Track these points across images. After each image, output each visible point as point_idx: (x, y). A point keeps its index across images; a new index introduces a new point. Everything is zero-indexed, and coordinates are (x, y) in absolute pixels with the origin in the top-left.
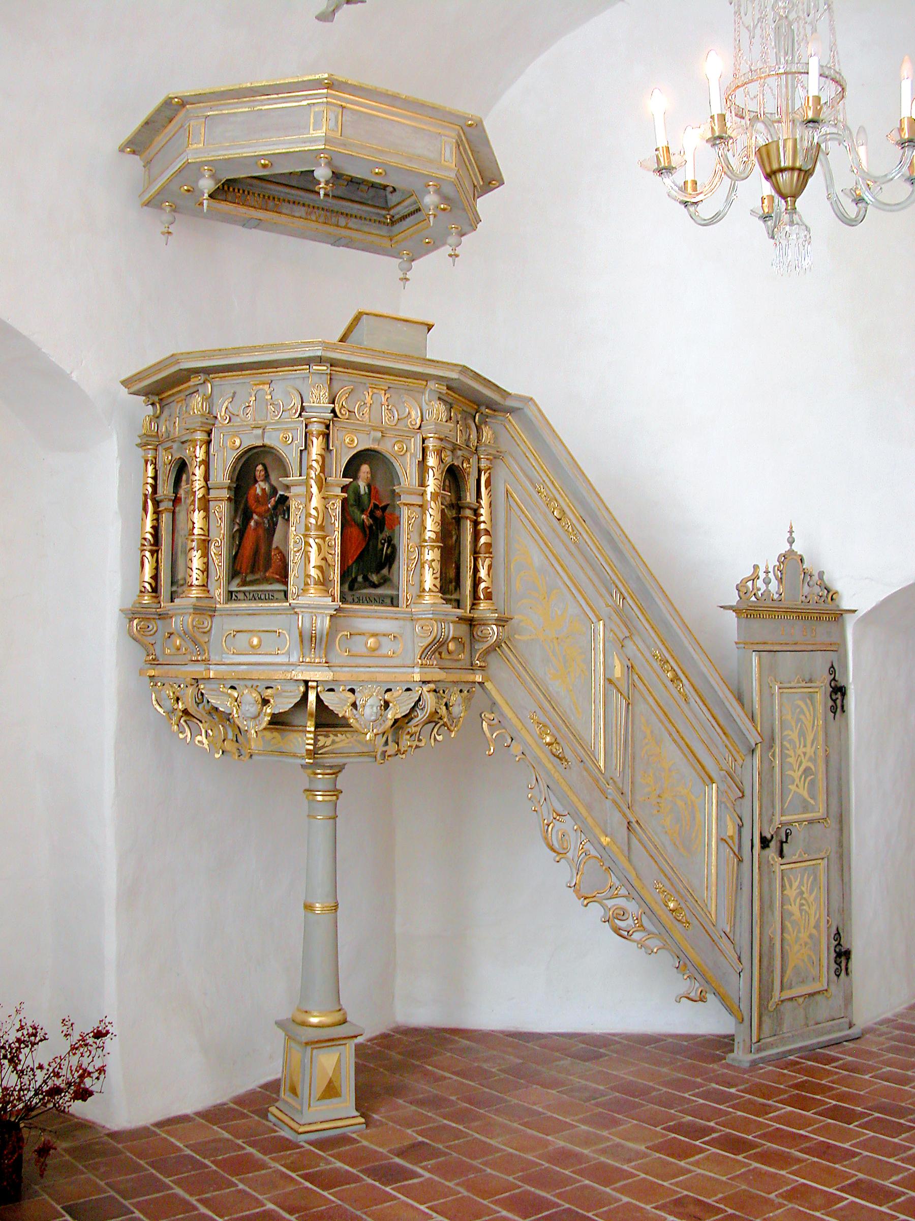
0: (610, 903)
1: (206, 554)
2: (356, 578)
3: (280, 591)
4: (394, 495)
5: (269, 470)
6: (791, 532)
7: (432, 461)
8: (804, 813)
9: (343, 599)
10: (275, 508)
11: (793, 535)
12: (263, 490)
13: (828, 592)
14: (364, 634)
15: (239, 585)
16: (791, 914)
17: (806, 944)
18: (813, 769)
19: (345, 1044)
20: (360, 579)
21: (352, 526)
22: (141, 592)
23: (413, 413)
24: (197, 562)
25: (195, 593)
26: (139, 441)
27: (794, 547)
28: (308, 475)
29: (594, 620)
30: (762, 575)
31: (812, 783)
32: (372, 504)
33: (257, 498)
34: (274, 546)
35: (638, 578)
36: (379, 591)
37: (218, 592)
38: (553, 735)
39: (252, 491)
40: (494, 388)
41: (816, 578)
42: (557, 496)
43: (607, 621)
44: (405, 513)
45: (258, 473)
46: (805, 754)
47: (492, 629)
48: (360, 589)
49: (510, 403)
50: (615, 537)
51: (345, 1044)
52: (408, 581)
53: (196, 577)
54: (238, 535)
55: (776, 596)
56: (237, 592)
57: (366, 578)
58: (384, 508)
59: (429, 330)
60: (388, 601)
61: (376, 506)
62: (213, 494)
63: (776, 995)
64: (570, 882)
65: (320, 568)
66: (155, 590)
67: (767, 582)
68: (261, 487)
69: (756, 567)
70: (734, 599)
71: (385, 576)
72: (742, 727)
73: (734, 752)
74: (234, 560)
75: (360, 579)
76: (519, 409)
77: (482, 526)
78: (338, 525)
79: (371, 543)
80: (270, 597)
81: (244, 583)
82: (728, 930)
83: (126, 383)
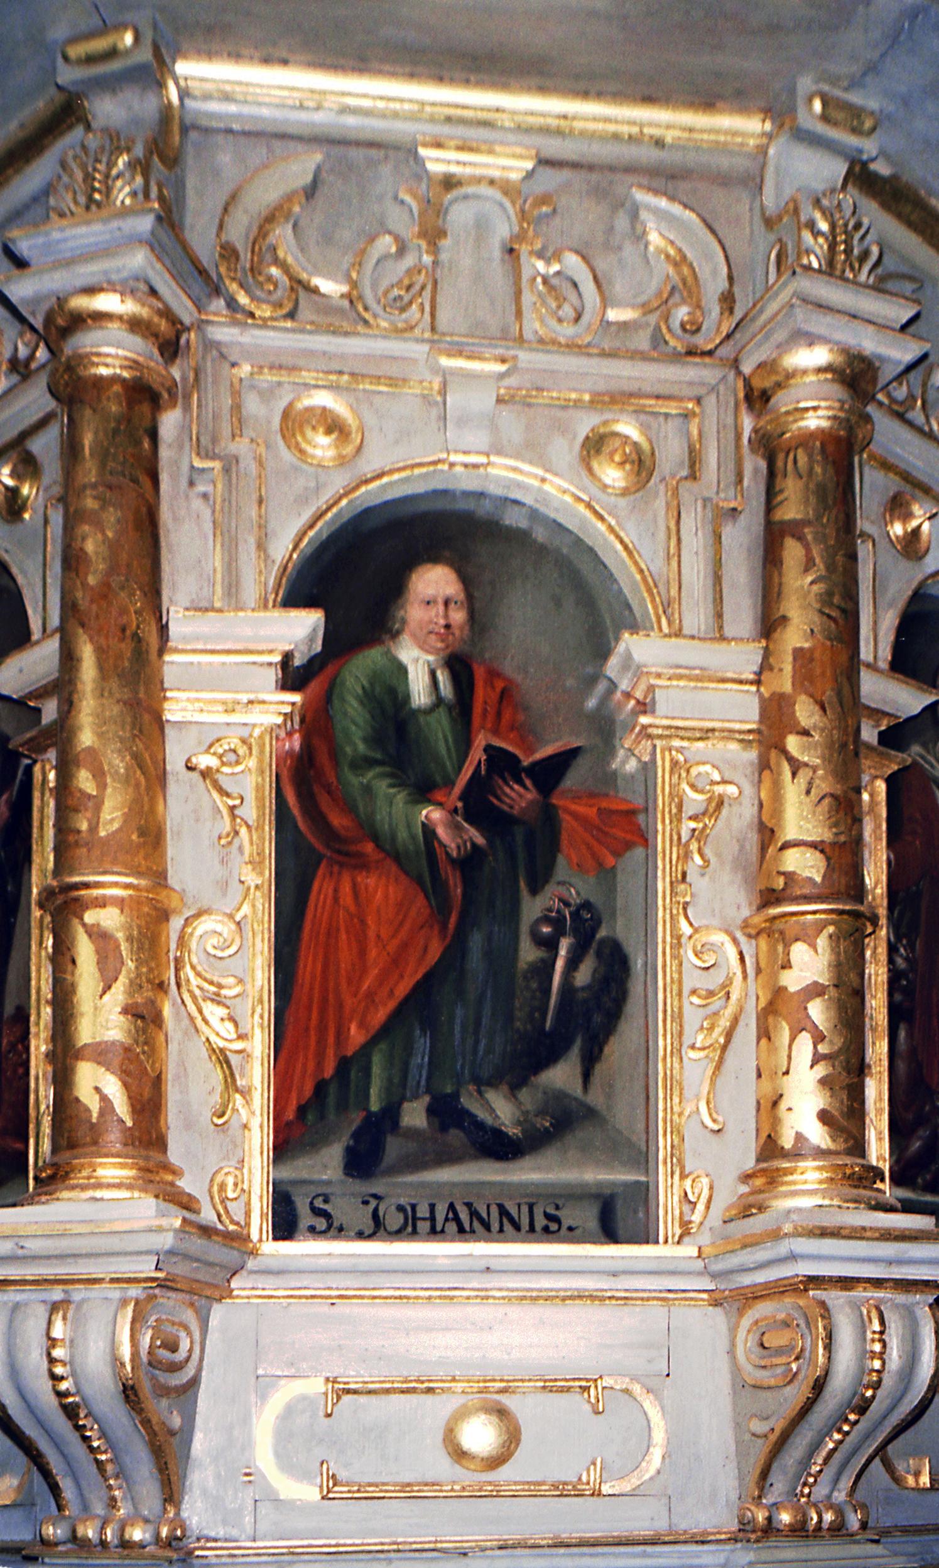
2: (391, 1114)
20: (414, 1115)
21: (361, 864)
32: (477, 754)
71: (560, 1096)
75: (414, 1115)
79: (476, 941)
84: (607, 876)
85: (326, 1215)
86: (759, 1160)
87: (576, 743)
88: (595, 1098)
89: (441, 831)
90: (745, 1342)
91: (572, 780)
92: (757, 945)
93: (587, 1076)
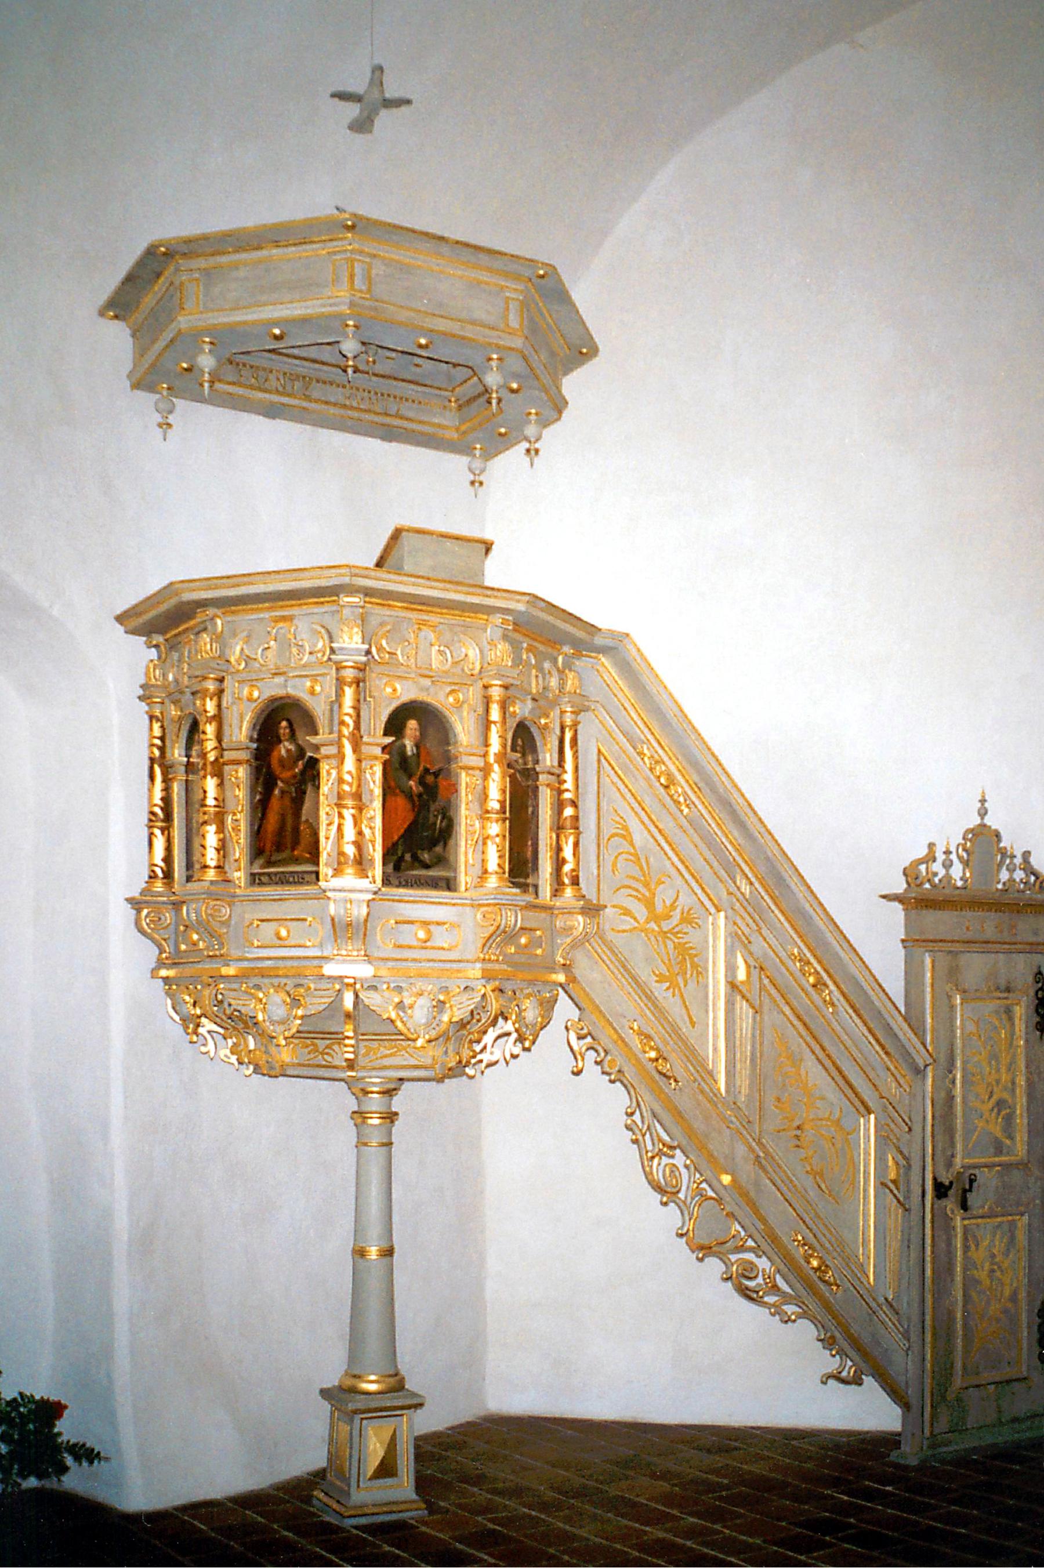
0: (733, 1258)
1: (221, 829)
2: (403, 856)
3: (311, 872)
4: (448, 758)
5: (295, 726)
6: (983, 801)
7: (495, 714)
8: (996, 1155)
9: (386, 881)
10: (303, 772)
11: (986, 805)
12: (288, 751)
13: (1037, 878)
14: (411, 922)
15: (262, 867)
16: (978, 1282)
17: (998, 1320)
18: (1010, 1101)
19: (402, 1415)
20: (408, 857)
21: (395, 795)
22: (150, 877)
23: (471, 653)
24: (211, 839)
25: (211, 874)
26: (141, 692)
27: (988, 821)
28: (340, 731)
29: (713, 910)
30: (940, 857)
31: (1009, 1119)
32: (421, 768)
33: (281, 760)
34: (303, 818)
35: (768, 859)
36: (432, 873)
37: (239, 876)
38: (658, 1050)
39: (275, 754)
40: (574, 621)
41: (1018, 860)
42: (666, 759)
43: (730, 911)
44: (464, 778)
45: (282, 731)
46: (998, 1082)
47: (577, 920)
48: (408, 869)
49: (599, 641)
50: (737, 808)
51: (402, 1415)
52: (466, 862)
53: (211, 857)
54: (261, 807)
55: (960, 884)
56: (260, 874)
57: (415, 858)
58: (436, 775)
59: (488, 550)
60: (443, 884)
61: (427, 771)
62: (228, 755)
63: (958, 1382)
64: (682, 1228)
65: (356, 843)
66: (168, 875)
67: (948, 865)
68: (285, 748)
69: (931, 846)
70: (900, 886)
72: (907, 1045)
73: (899, 1077)
74: (257, 834)
75: (408, 857)
76: (615, 648)
77: (567, 795)
78: (378, 791)
80: (299, 880)
81: (269, 863)
82: (890, 1297)
83: (120, 619)
86: (141, 894)
90: (479, 916)
92: (382, 92)
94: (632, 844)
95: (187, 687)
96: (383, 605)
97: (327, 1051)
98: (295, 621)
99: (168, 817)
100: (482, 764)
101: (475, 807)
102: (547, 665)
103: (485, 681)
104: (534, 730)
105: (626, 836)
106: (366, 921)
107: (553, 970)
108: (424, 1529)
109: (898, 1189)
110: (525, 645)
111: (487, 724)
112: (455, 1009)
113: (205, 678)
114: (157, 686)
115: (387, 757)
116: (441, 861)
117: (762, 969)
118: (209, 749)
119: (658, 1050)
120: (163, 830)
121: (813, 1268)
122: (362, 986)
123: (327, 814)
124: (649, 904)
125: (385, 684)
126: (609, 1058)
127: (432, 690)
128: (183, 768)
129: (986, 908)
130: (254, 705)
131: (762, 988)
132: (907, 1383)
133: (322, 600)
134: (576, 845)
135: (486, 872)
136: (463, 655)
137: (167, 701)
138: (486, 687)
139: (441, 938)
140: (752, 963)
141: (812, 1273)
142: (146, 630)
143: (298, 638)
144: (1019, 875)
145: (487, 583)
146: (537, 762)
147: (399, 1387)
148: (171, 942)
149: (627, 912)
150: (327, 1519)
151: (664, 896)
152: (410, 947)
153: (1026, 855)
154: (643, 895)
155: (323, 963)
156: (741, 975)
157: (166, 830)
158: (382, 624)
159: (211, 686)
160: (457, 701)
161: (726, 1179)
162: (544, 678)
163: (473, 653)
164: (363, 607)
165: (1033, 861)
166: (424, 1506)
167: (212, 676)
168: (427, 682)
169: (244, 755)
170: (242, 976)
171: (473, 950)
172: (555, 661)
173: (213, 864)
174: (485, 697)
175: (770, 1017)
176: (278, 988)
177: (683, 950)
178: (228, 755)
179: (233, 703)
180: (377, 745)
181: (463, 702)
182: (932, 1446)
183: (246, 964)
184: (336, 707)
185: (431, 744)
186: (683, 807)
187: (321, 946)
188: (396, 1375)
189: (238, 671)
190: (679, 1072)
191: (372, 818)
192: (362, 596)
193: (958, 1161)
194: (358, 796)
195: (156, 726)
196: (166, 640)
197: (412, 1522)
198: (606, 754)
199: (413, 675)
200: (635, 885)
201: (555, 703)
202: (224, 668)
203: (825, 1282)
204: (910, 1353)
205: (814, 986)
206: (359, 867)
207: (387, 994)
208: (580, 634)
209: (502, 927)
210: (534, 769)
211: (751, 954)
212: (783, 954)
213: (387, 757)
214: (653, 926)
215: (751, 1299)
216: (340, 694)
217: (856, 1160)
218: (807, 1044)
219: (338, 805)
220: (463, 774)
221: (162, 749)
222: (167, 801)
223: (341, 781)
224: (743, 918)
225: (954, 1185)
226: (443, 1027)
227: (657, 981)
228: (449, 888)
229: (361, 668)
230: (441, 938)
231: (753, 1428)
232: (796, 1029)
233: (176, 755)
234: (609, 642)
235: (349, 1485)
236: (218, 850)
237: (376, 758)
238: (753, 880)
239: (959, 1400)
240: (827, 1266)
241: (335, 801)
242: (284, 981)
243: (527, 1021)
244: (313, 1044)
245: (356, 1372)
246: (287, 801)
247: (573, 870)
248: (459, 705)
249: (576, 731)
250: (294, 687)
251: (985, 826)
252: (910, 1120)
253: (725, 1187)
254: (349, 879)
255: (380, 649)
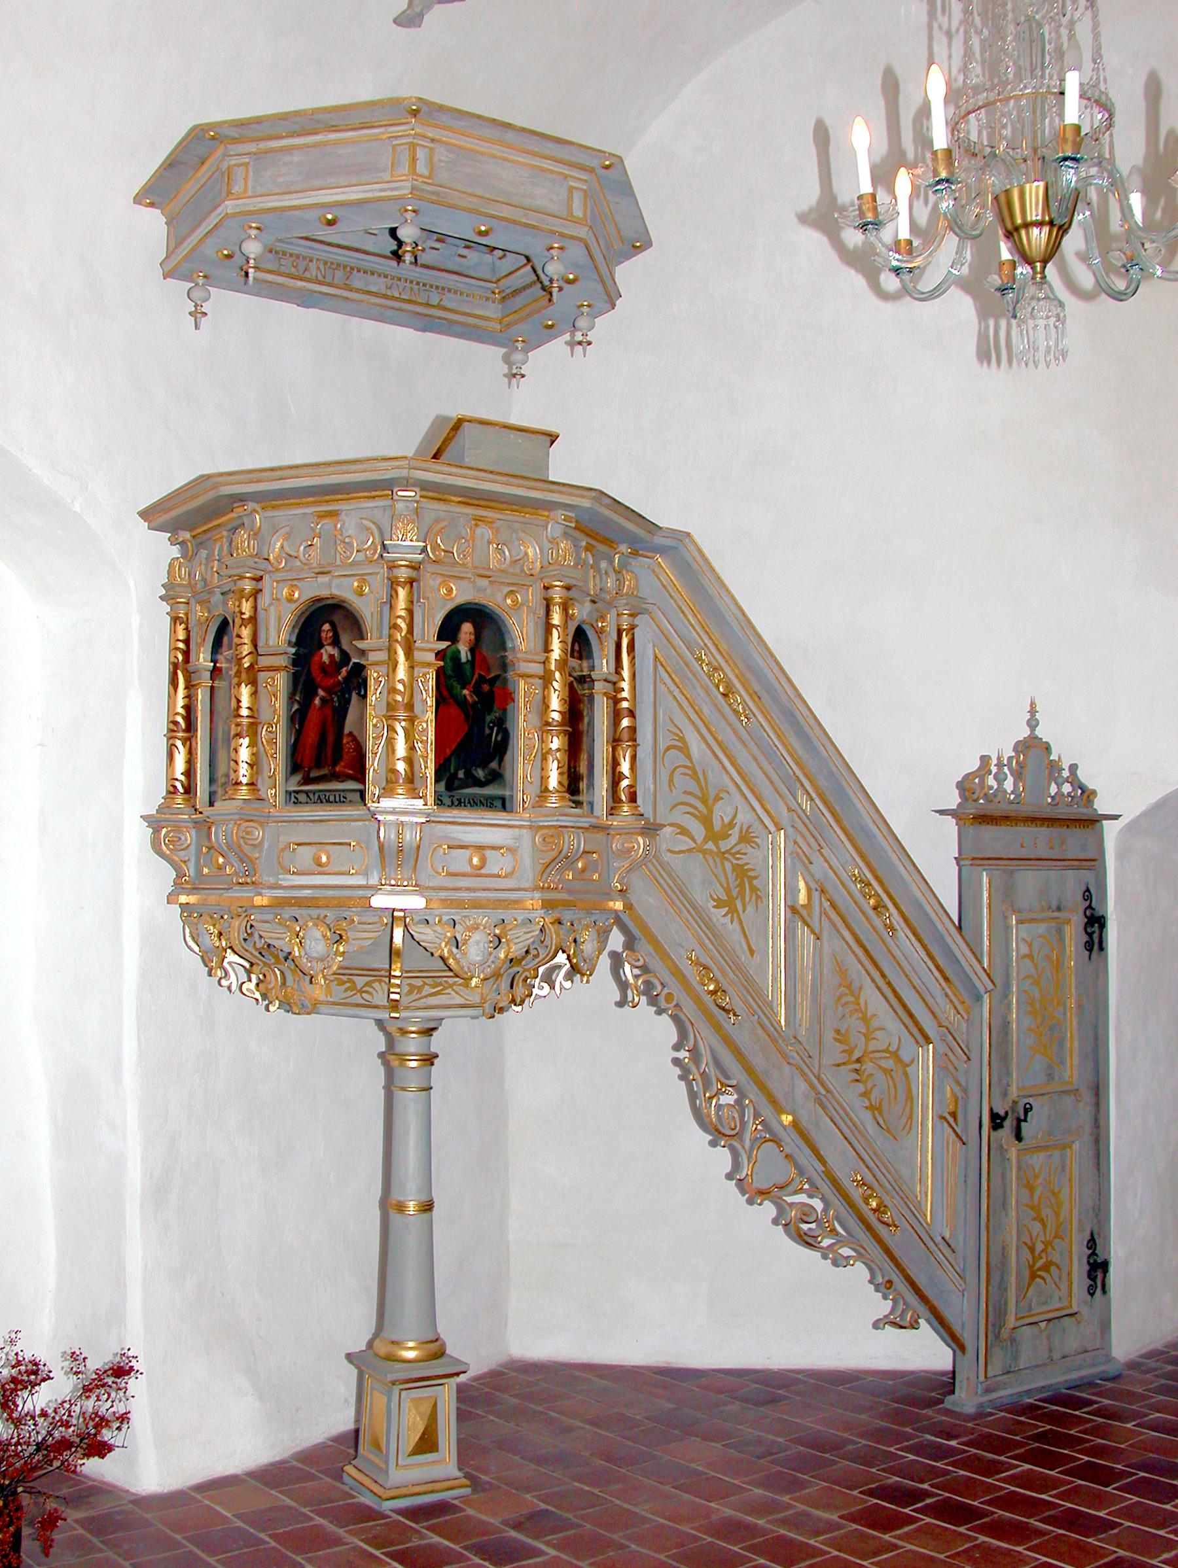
2: (456, 773)
4: (504, 666)
7: (556, 619)
9: (439, 802)
12: (331, 657)
15: (300, 784)
20: (461, 774)
22: (169, 792)
23: (530, 552)
27: (1039, 732)
32: (476, 676)
33: (323, 666)
34: (346, 731)
35: (831, 773)
40: (631, 515)
41: (1065, 774)
43: (790, 830)
45: (323, 635)
49: (658, 540)
57: (468, 774)
59: (552, 442)
60: (498, 803)
61: (482, 679)
63: (1011, 1321)
66: (189, 790)
67: (1000, 779)
68: (328, 652)
69: (985, 760)
70: (953, 800)
75: (461, 774)
80: (340, 799)
81: (307, 781)
82: (947, 1236)
83: (145, 514)
84: (505, 710)
85: (441, 801)
87: (498, 673)
88: (501, 771)
89: (468, 697)
91: (498, 684)
93: (500, 767)
94: (689, 758)
95: (218, 587)
96: (440, 500)
97: (367, 988)
98: (343, 516)
99: (190, 726)
100: (541, 672)
101: (535, 720)
102: (604, 565)
103: (546, 582)
104: (591, 634)
105: (684, 749)
106: (419, 847)
107: (608, 896)
108: (470, 1512)
109: (955, 1120)
110: (584, 544)
111: (548, 627)
112: (512, 945)
113: (242, 578)
114: (182, 585)
115: (442, 663)
116: (496, 777)
117: (822, 891)
118: (245, 653)
119: (717, 982)
120: (185, 741)
121: (872, 1209)
122: (412, 920)
123: (375, 726)
124: (707, 821)
125: (440, 584)
126: (666, 991)
127: (489, 591)
128: (208, 674)
129: (1039, 823)
130: (296, 605)
131: (823, 912)
132: (963, 1324)
133: (374, 494)
134: (634, 758)
135: (546, 790)
136: (522, 554)
137: (193, 601)
138: (546, 588)
139: (497, 863)
140: (813, 885)
141: (871, 1213)
142: (172, 527)
143: (345, 534)
144: (1067, 788)
145: (550, 479)
146: (592, 668)
147: (440, 1354)
148: (192, 865)
149: (684, 831)
150: (362, 1499)
151: (721, 813)
152: (464, 875)
153: (1073, 768)
154: (700, 812)
155: (369, 893)
156: (802, 898)
157: (189, 741)
158: (437, 521)
159: (248, 586)
160: (515, 602)
161: (787, 1119)
162: (601, 579)
163: (532, 551)
164: (417, 502)
165: (1080, 773)
166: (468, 1482)
167: (248, 575)
168: (484, 583)
169: (283, 661)
170: (278, 904)
171: (528, 873)
172: (611, 562)
173: (244, 780)
174: (545, 599)
175: (831, 944)
176: (319, 921)
177: (742, 872)
178: (264, 661)
179: (272, 604)
180: (430, 650)
181: (522, 605)
182: (988, 1390)
183: (280, 893)
184: (386, 608)
185: (486, 650)
186: (742, 718)
187: (366, 874)
188: (437, 1340)
189: (277, 570)
190: (739, 1006)
191: (425, 730)
192: (417, 489)
193: (1014, 1092)
194: (410, 707)
195: (180, 628)
196: (194, 537)
197: (456, 1502)
198: (662, 659)
199: (469, 576)
200: (693, 801)
201: (610, 604)
202: (262, 567)
203: (884, 1223)
204: (965, 1293)
205: (875, 908)
206: (410, 786)
207: (438, 928)
208: (641, 533)
209: (564, 851)
210: (590, 676)
211: (812, 875)
212: (844, 876)
213: (442, 663)
214: (710, 845)
215: (809, 1245)
216: (393, 595)
217: (914, 1092)
218: (867, 971)
219: (388, 718)
220: (522, 683)
221: (186, 654)
222: (189, 709)
223: (393, 690)
224: (804, 837)
225: (1010, 1113)
226: (498, 963)
227: (714, 907)
228: (504, 808)
229: (415, 567)
230: (497, 863)
231: (785, 1370)
232: (856, 955)
233: (201, 660)
234: (669, 542)
235: (387, 1463)
236: (251, 765)
237: (429, 665)
238: (814, 795)
239: (1013, 1340)
240: (885, 1206)
241: (384, 712)
242: (323, 912)
243: (585, 955)
244: (349, 981)
245: (394, 1338)
246: (328, 712)
247: (630, 786)
248: (516, 606)
249: (633, 634)
250: (338, 587)
251: (1037, 737)
252: (967, 1046)
253: (784, 1127)
254: (400, 801)
255: (435, 547)
